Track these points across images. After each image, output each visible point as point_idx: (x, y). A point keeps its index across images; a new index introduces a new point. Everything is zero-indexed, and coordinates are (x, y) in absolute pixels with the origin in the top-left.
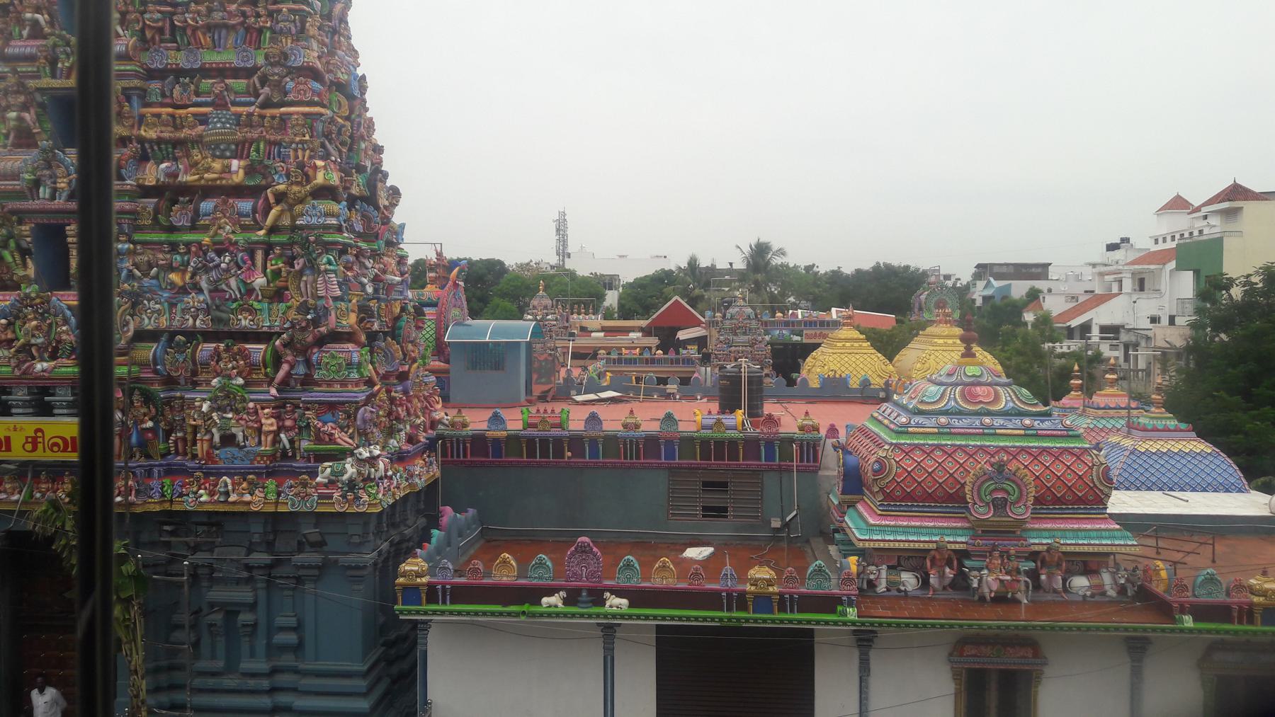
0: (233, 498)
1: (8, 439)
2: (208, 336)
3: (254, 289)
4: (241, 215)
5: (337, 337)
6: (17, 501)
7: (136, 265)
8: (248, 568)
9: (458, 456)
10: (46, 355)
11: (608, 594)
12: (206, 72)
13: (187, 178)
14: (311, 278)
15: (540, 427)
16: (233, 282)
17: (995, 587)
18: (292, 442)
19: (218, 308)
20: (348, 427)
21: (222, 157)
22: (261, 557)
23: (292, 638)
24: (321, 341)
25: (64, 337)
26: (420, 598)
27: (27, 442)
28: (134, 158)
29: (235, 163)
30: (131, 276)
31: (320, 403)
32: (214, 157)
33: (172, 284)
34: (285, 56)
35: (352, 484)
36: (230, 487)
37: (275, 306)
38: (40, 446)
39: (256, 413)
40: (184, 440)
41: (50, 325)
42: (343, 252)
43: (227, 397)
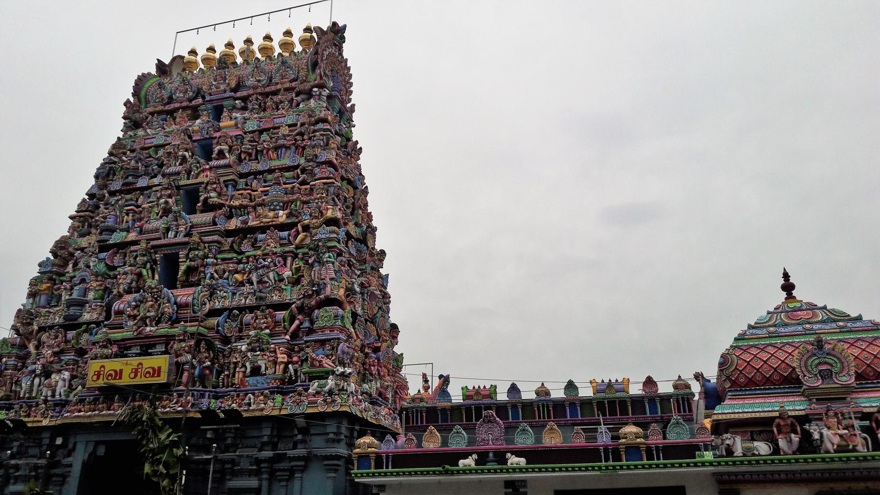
0: (253, 407)
1: (121, 371)
2: (251, 309)
4: (281, 239)
5: (331, 302)
7: (216, 271)
8: (258, 461)
9: (417, 423)
11: (509, 455)
12: (271, 171)
13: (252, 223)
14: (318, 268)
15: (475, 398)
16: (271, 275)
17: (837, 440)
18: (296, 371)
19: (260, 291)
20: (332, 355)
21: (274, 210)
22: (267, 454)
24: (321, 305)
25: (166, 310)
26: (370, 463)
29: (281, 213)
30: (212, 277)
31: (316, 341)
32: (270, 210)
35: (330, 393)
38: (139, 374)
39: (275, 352)
40: (228, 376)
42: (340, 254)
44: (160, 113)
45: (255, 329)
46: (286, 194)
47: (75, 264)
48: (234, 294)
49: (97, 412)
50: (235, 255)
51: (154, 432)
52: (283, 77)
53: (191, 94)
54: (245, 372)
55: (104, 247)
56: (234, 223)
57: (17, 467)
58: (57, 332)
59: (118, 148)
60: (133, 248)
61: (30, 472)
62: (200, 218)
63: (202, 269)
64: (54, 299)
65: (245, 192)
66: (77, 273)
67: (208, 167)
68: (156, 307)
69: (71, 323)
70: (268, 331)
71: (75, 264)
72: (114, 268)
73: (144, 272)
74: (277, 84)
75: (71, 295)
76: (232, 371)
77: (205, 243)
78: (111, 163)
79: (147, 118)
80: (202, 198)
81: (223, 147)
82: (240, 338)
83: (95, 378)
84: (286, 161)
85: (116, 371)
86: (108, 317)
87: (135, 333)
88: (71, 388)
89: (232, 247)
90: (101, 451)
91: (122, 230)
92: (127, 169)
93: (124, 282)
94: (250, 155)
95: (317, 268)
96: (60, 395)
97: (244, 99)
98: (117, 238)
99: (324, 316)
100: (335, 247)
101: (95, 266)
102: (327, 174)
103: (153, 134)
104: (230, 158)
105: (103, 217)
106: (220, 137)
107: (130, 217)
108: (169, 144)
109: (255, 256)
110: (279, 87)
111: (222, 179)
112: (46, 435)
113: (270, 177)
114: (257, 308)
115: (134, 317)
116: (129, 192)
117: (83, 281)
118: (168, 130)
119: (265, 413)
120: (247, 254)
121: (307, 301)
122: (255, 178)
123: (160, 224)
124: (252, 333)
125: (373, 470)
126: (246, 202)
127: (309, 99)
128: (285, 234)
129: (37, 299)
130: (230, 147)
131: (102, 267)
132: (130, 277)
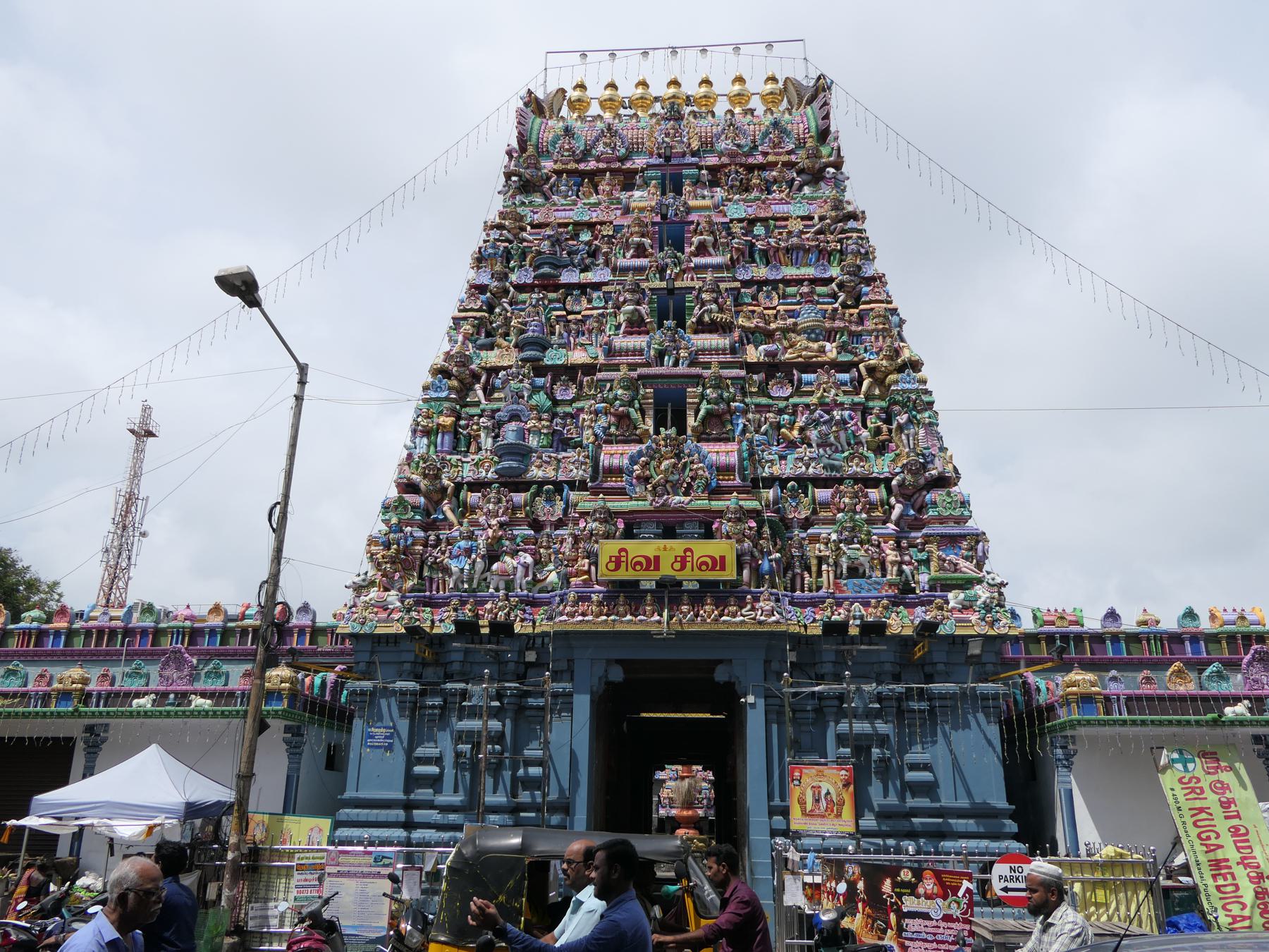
1: (657, 558)
29: (828, 346)
31: (942, 536)
34: (859, 268)
38: (689, 565)
44: (570, 173)
58: (498, 492)
64: (461, 441)
78: (502, 241)
97: (713, 170)
116: (545, 288)
128: (845, 377)
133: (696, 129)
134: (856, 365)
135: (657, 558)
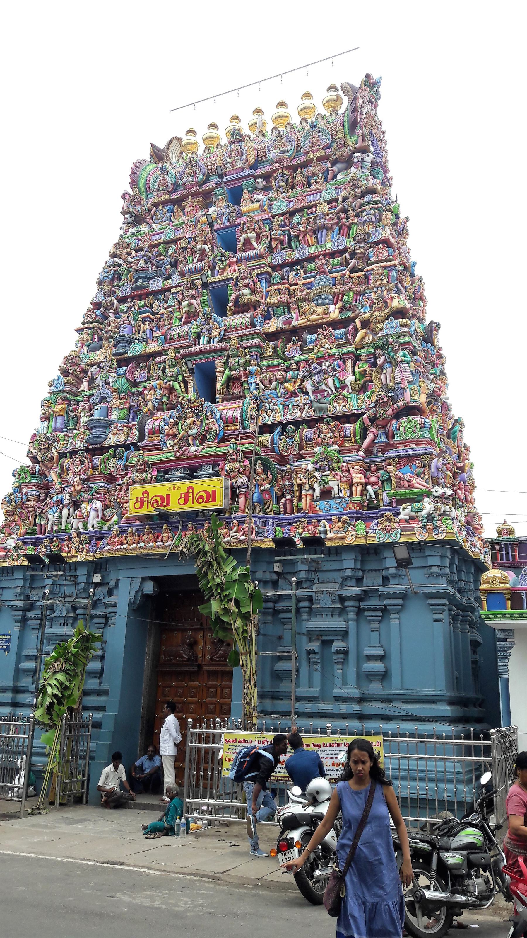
1: (168, 496)
2: (310, 423)
3: (347, 386)
4: (337, 338)
5: (412, 410)
6: (170, 545)
7: (261, 381)
8: (342, 599)
10: (197, 442)
12: (311, 259)
14: (389, 370)
16: (330, 381)
18: (376, 493)
19: (319, 401)
20: (424, 474)
21: (323, 305)
23: (378, 666)
25: (211, 426)
26: (505, 603)
27: (181, 497)
28: (262, 315)
29: (332, 307)
31: (400, 458)
32: (318, 305)
33: (287, 390)
35: (430, 517)
36: (328, 528)
37: (361, 396)
38: (190, 499)
39: (348, 471)
41: (202, 422)
43: (326, 458)
44: (165, 203)
45: (319, 445)
46: (335, 284)
47: (92, 381)
48: (285, 406)
49: (142, 544)
50: (281, 361)
51: (219, 564)
52: (313, 144)
53: (201, 177)
54: (313, 495)
55: (123, 361)
56: (274, 325)
57: (52, 608)
58: (83, 457)
59: (120, 249)
60: (158, 359)
61: (68, 613)
62: (231, 320)
63: (244, 379)
65: (283, 287)
66: (95, 391)
67: (235, 259)
68: (199, 423)
69: (96, 449)
70: (336, 447)
71: (92, 381)
72: (135, 384)
73: (176, 385)
74: (307, 153)
75: (91, 415)
76: (296, 494)
77: (244, 348)
78: (114, 266)
79: (150, 211)
80: (233, 296)
81: (249, 235)
82: (300, 457)
83: (138, 505)
84: (329, 244)
85: (162, 497)
86: (141, 438)
87: (178, 454)
88: (105, 519)
89: (275, 351)
90: (149, 588)
91: (141, 340)
92: (136, 270)
93: (152, 398)
94: (282, 242)
95: (388, 370)
96: (93, 527)
97: (267, 177)
98: (135, 349)
99: (406, 426)
100: (409, 343)
101: (115, 382)
102: (385, 256)
103: (161, 229)
104: (259, 248)
105: (115, 327)
106: (245, 224)
107: (147, 326)
108: (181, 238)
109: (307, 361)
110: (310, 156)
111: (254, 273)
112: (82, 571)
113: (310, 266)
114: (320, 420)
115: (175, 436)
116: (140, 297)
117: (103, 399)
118: (176, 222)
119: (347, 542)
120: (296, 359)
121: (380, 411)
122: (291, 270)
123: (189, 329)
124: (317, 450)
125: (510, 610)
126: (285, 298)
127: (348, 168)
128: (341, 332)
129: (52, 422)
130: (258, 235)
131: (123, 383)
132: (158, 392)
133: (175, 164)
134: (353, 320)
135: (168, 496)
